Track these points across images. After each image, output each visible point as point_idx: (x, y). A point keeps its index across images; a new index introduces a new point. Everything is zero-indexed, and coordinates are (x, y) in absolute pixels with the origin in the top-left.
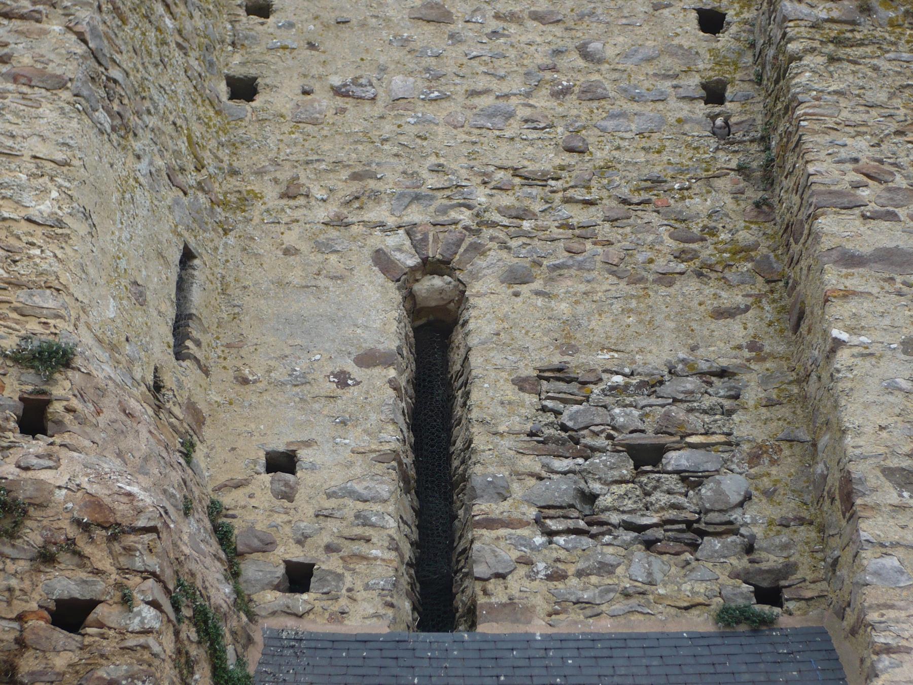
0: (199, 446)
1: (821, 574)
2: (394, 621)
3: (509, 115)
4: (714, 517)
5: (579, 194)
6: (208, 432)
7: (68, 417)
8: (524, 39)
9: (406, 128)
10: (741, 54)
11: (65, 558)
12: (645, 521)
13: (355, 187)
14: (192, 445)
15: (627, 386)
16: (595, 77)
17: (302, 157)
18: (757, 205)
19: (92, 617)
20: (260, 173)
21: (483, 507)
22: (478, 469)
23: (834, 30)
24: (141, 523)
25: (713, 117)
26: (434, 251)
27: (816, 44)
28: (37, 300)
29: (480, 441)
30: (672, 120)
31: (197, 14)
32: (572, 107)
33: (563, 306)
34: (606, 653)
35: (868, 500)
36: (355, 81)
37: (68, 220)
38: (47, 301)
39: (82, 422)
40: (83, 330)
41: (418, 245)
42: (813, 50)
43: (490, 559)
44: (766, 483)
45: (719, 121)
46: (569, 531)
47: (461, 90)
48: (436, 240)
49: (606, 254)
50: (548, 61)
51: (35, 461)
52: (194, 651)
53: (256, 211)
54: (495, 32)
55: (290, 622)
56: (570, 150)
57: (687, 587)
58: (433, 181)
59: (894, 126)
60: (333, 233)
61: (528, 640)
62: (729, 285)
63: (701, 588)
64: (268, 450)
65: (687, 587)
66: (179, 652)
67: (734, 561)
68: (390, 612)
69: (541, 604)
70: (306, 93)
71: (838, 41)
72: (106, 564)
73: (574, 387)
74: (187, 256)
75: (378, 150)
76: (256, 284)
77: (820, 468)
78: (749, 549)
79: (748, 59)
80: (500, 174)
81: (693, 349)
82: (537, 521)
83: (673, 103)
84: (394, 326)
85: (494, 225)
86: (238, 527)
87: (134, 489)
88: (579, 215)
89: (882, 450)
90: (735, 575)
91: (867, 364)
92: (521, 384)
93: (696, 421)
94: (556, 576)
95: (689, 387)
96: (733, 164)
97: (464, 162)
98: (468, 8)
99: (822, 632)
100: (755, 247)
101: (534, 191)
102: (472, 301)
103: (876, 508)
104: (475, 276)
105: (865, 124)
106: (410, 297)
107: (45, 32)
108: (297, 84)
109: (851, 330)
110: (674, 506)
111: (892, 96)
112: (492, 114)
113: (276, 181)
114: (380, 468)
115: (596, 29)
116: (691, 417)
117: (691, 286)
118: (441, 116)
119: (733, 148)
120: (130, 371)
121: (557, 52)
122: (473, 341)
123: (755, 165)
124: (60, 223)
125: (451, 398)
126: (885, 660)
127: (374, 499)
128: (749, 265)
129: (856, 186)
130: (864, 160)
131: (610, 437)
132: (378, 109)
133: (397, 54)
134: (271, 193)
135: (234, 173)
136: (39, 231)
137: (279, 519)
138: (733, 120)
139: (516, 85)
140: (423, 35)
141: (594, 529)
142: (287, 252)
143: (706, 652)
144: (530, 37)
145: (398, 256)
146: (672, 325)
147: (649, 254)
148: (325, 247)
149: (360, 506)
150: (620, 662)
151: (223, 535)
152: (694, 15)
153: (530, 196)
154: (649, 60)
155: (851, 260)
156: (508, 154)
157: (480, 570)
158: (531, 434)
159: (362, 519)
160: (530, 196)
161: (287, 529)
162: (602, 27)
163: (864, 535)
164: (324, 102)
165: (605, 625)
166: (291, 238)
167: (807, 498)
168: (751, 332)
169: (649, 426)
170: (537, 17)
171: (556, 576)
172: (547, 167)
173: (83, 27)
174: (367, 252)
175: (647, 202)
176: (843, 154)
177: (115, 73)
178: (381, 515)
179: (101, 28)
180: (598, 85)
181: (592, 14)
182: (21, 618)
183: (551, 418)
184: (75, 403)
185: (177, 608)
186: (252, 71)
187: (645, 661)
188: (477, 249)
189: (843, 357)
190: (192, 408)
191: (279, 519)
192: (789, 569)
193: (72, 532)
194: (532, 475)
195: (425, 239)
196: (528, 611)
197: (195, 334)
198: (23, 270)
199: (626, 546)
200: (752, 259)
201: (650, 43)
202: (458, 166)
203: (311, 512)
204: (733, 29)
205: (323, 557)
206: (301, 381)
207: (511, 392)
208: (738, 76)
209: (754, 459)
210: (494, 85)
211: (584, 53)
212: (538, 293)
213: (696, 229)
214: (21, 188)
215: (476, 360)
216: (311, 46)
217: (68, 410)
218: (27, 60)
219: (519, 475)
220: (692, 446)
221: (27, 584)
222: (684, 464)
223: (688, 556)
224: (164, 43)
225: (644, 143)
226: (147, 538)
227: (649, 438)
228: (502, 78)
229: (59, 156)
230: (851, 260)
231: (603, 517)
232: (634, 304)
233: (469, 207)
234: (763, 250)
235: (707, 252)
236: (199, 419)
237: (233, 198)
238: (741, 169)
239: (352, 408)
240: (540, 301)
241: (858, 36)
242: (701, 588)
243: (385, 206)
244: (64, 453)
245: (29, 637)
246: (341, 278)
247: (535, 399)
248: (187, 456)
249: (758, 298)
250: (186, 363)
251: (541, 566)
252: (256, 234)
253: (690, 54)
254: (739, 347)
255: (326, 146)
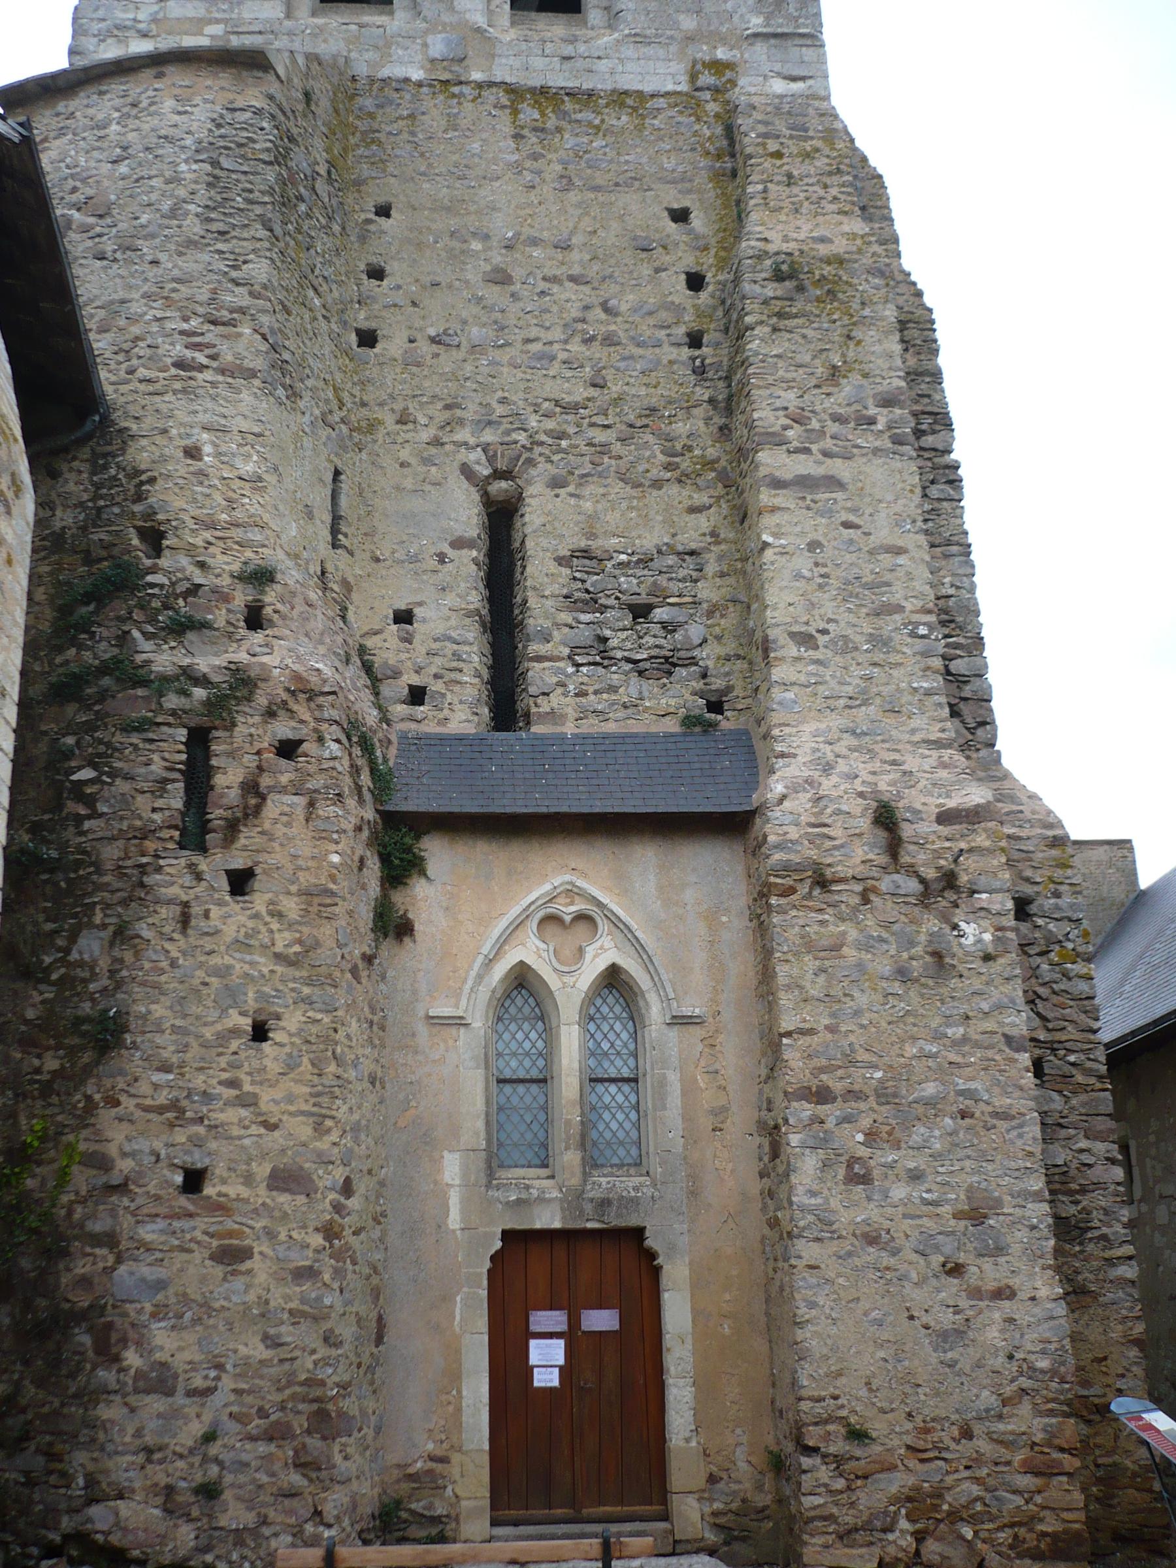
0: (350, 607)
1: (749, 693)
2: (479, 724)
3: (553, 358)
4: (683, 654)
5: (600, 420)
6: (355, 596)
7: (276, 616)
8: (563, 297)
9: (481, 369)
10: (715, 308)
11: (281, 713)
12: (639, 657)
13: (447, 415)
14: (346, 609)
15: (629, 562)
16: (613, 327)
17: (410, 392)
18: (721, 429)
19: (300, 750)
20: (381, 405)
21: (535, 648)
22: (531, 621)
23: (777, 306)
24: (326, 689)
25: (693, 359)
26: (502, 465)
27: (765, 318)
28: (250, 536)
29: (532, 602)
30: (665, 362)
31: (334, 287)
32: (597, 351)
33: (588, 504)
34: (611, 747)
35: (778, 654)
36: (445, 332)
37: (265, 476)
38: (255, 535)
39: (284, 618)
40: (279, 550)
41: (491, 460)
42: (762, 322)
43: (539, 682)
44: (717, 630)
45: (698, 362)
46: (590, 664)
47: (519, 338)
48: (503, 456)
49: (618, 466)
50: (579, 315)
51: (258, 649)
52: (360, 762)
53: (380, 434)
54: (542, 292)
55: (413, 726)
56: (594, 385)
57: (663, 701)
58: (500, 410)
59: (814, 382)
60: (433, 450)
61: (562, 738)
62: (699, 488)
63: (672, 702)
64: (396, 607)
65: (663, 701)
66: (352, 766)
67: (694, 683)
68: (476, 718)
69: (571, 713)
70: (411, 341)
71: (780, 315)
72: (307, 716)
73: (594, 563)
74: (337, 473)
75: (462, 386)
76: (383, 489)
77: (751, 624)
78: (704, 676)
79: (720, 313)
80: (546, 405)
81: (674, 535)
82: (569, 657)
83: (666, 348)
84: (475, 520)
85: (542, 443)
86: (377, 661)
87: (320, 666)
88: (600, 436)
89: (789, 620)
90: (694, 693)
91: (783, 559)
92: (560, 561)
93: (674, 587)
94: (581, 694)
95: (670, 562)
96: (706, 397)
97: (521, 395)
98: (524, 272)
99: (746, 732)
100: (718, 460)
101: (570, 418)
102: (527, 500)
103: (782, 659)
104: (529, 482)
105: (794, 380)
106: (485, 495)
107: (240, 335)
108: (405, 334)
109: (776, 535)
110: (657, 646)
111: (814, 357)
112: (540, 357)
113: (392, 410)
114: (468, 621)
115: (614, 288)
116: (671, 584)
117: (674, 489)
118: (506, 359)
119: (708, 384)
120: (307, 569)
121: (586, 308)
122: (528, 530)
123: (720, 397)
124: (260, 479)
125: (512, 565)
126: (781, 762)
127: (465, 643)
128: (714, 474)
129: (785, 428)
130: (791, 409)
131: (617, 598)
132: (462, 354)
133: (475, 310)
134: (389, 420)
135: (364, 404)
136: (248, 485)
137: (404, 656)
138: (707, 361)
139: (557, 334)
140: (493, 294)
141: (606, 662)
142: (402, 465)
143: (673, 746)
144: (566, 295)
145: (477, 468)
146: (660, 518)
147: (646, 466)
148: (427, 461)
149: (455, 647)
150: (620, 754)
151: (368, 668)
152: (683, 277)
153: (566, 422)
154: (650, 313)
155: (778, 484)
156: (552, 389)
157: (532, 690)
158: (566, 597)
159: (457, 656)
160: (566, 422)
161: (409, 664)
162: (618, 288)
163: (774, 678)
164: (424, 348)
165: (611, 727)
166: (405, 454)
167: (743, 641)
168: (712, 523)
169: (643, 590)
170: (573, 279)
171: (581, 694)
172: (578, 399)
173: (265, 330)
174: (456, 465)
175: (646, 426)
176: (778, 403)
177: (286, 356)
178: (469, 654)
179: (276, 325)
180: (614, 333)
181: (611, 277)
182: (258, 753)
183: (580, 585)
184: (279, 606)
185: (349, 739)
186: (373, 325)
187: (635, 754)
188: (530, 462)
189: (769, 554)
190: (346, 584)
191: (404, 656)
192: (729, 689)
193: (285, 696)
194: (566, 625)
195: (495, 455)
196: (563, 717)
197: (344, 529)
198: (239, 514)
199: (626, 674)
200: (714, 470)
201: (652, 300)
202: (517, 397)
203: (424, 651)
204: (711, 288)
205: (432, 682)
206: (414, 559)
207: (553, 567)
208: (712, 326)
209: (710, 614)
210: (543, 334)
211: (607, 310)
212: (572, 495)
213: (678, 447)
214: (233, 455)
215: (529, 544)
216: (414, 304)
217: (275, 612)
218: (230, 358)
219: (557, 625)
220: (669, 604)
221: (260, 732)
222: (665, 617)
223: (665, 680)
224: (315, 319)
225: (645, 380)
226: (331, 698)
227: (643, 599)
228: (548, 328)
229: (256, 430)
230: (778, 484)
231: (612, 654)
232: (635, 502)
233: (525, 430)
234: (723, 463)
235: (685, 464)
236: (347, 586)
237: (364, 424)
238: (711, 401)
239: (448, 579)
240: (572, 501)
241: (794, 310)
242: (672, 702)
243: (468, 429)
244: (275, 642)
245: (265, 765)
246: (439, 484)
247: (568, 571)
248: (343, 618)
249: (719, 498)
250: (339, 551)
251: (571, 687)
252: (381, 452)
253: (678, 309)
254: (704, 535)
255: (427, 384)
